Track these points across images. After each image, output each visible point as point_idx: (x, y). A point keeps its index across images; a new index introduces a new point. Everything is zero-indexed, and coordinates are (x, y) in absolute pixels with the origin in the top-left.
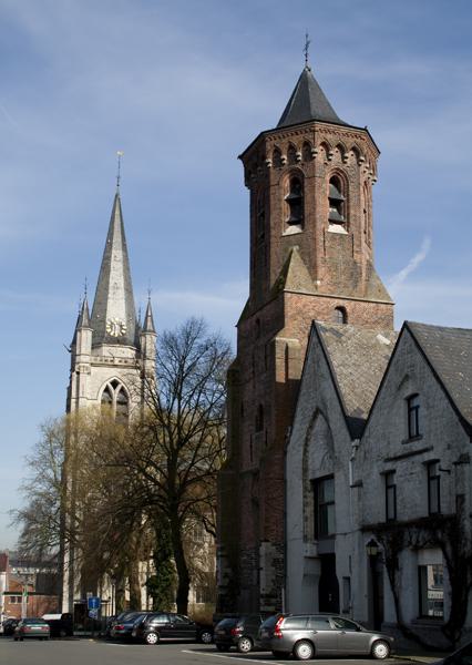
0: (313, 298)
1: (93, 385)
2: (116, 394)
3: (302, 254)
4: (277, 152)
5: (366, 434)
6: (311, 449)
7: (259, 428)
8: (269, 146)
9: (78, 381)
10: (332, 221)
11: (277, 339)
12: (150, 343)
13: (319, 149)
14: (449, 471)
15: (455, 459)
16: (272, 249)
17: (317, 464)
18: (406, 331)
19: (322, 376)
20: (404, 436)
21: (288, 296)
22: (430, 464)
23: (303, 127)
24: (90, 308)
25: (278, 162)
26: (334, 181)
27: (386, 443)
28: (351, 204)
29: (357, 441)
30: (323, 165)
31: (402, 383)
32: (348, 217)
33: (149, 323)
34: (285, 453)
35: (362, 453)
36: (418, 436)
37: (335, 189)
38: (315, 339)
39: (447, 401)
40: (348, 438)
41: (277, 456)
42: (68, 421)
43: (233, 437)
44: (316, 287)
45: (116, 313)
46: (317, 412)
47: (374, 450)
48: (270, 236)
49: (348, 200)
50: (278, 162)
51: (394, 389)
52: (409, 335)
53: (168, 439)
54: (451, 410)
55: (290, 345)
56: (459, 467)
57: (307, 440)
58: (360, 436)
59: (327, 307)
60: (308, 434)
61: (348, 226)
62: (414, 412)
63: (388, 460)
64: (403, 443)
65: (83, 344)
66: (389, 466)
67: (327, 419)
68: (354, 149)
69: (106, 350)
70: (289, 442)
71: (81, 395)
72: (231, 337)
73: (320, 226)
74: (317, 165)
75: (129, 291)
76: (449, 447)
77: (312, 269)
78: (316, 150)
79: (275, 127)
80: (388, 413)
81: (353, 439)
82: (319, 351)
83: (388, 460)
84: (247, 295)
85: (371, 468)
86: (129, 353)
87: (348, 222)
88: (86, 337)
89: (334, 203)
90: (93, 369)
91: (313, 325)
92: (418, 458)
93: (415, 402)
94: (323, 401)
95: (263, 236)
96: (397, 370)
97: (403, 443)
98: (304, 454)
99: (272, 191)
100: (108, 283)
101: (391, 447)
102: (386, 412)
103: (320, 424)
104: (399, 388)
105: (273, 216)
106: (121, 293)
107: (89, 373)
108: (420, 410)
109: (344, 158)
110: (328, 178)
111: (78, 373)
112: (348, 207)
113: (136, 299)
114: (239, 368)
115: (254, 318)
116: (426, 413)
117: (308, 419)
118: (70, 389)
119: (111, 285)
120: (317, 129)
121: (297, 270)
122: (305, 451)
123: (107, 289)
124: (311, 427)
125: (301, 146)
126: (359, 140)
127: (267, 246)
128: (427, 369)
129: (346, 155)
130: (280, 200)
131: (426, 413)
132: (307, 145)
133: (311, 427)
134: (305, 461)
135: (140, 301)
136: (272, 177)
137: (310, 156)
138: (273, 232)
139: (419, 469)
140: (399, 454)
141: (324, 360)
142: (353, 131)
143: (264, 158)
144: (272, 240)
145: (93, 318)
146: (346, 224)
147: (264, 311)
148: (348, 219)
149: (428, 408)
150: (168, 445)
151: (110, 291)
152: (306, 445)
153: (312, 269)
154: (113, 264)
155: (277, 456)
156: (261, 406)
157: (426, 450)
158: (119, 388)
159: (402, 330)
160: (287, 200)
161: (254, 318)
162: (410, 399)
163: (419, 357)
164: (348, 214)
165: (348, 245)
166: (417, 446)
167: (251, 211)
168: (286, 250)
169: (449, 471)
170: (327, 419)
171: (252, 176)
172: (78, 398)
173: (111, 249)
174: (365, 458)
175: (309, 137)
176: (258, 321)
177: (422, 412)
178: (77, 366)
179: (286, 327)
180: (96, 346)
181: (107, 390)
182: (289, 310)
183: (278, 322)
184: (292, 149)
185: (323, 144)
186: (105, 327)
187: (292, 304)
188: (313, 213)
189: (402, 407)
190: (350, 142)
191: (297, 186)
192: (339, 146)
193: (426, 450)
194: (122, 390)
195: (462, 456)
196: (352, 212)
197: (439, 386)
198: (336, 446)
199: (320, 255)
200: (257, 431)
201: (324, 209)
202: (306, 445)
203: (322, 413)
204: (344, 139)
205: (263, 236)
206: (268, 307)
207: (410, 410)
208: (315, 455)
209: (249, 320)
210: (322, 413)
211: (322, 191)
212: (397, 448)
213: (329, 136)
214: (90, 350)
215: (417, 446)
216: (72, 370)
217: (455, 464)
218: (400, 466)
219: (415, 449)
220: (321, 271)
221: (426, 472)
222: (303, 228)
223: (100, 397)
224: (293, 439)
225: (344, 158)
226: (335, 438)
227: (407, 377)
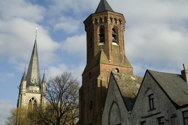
0: (108, 65)
1: (26, 98)
2: (33, 102)
3: (105, 52)
4: (96, 20)
5: (134, 109)
6: (111, 115)
7: (91, 108)
8: (93, 18)
9: (21, 98)
10: (113, 41)
11: (98, 78)
12: (44, 86)
13: (109, 19)
14: (168, 121)
15: (171, 116)
16: (95, 50)
17: (114, 120)
18: (147, 72)
19: (115, 90)
20: (148, 109)
21: (101, 64)
22: (159, 119)
23: (104, 13)
24: (26, 75)
25: (96, 23)
26: (113, 29)
27: (142, 112)
28: (119, 36)
29: (130, 112)
30: (111, 25)
31: (147, 90)
32: (118, 40)
33: (44, 80)
34: (101, 117)
35: (132, 116)
36: (154, 109)
37: (113, 32)
38: (112, 78)
39: (165, 96)
40: (126, 111)
41: (99, 118)
42: (17, 111)
43: (81, 112)
44: (109, 62)
45: (34, 76)
46: (114, 102)
47: (137, 115)
48: (94, 46)
49: (118, 35)
50: (96, 23)
51: (144, 93)
52: (149, 74)
53: (57, 114)
54: (167, 98)
55: (102, 80)
56: (173, 119)
57: (110, 112)
58: (131, 110)
59: (113, 68)
60: (110, 110)
61: (118, 43)
62: (151, 101)
63: (143, 118)
64: (148, 111)
65: (24, 86)
66: (143, 120)
67: (118, 105)
68: (119, 20)
69: (30, 88)
70: (103, 113)
71: (22, 102)
72: (80, 80)
73: (110, 43)
74: (108, 24)
75: (38, 70)
76: (168, 112)
77: (108, 56)
78: (108, 20)
79: (94, 12)
80: (142, 101)
81: (128, 111)
82: (114, 81)
83: (143, 118)
84: (86, 64)
85: (136, 121)
86: (38, 89)
87: (118, 42)
88: (25, 83)
89: (114, 36)
90: (26, 94)
91: (112, 73)
92: (155, 116)
93: (152, 97)
94: (116, 98)
95: (91, 46)
96: (144, 86)
97: (148, 111)
98: (109, 117)
99: (95, 31)
100: (32, 67)
101: (143, 113)
102: (141, 101)
103: (115, 106)
104: (146, 92)
105: (95, 39)
106: (36, 70)
107: (25, 95)
108: (154, 100)
109: (116, 22)
110: (112, 28)
111: (22, 95)
112: (118, 37)
113: (40, 72)
114: (83, 89)
115: (89, 72)
116: (157, 100)
117: (110, 105)
118: (19, 99)
119: (33, 68)
120: (108, 13)
121: (103, 57)
122: (109, 116)
123: (32, 69)
124: (111, 107)
125: (103, 18)
126: (120, 17)
127: (93, 49)
128: (157, 85)
129: (117, 21)
130: (97, 35)
131: (157, 100)
132: (106, 18)
133: (111, 107)
134: (109, 119)
135: (42, 72)
136: (94, 28)
137: (106, 21)
138: (95, 45)
139: (156, 120)
140: (146, 116)
141: (116, 84)
142: (119, 15)
143: (92, 22)
144: (95, 47)
145: (27, 77)
146: (118, 43)
147: (92, 70)
148: (118, 41)
149: (158, 98)
150: (57, 116)
151: (33, 69)
152: (109, 114)
153: (108, 56)
154: (34, 61)
155: (99, 118)
156: (91, 101)
157: (158, 113)
158: (34, 100)
159: (146, 72)
160: (99, 35)
161: (89, 72)
162: (149, 96)
163: (153, 81)
164: (118, 39)
165: (119, 49)
166: (154, 112)
167: (87, 38)
168: (100, 50)
169: (168, 121)
170: (118, 105)
171: (88, 27)
172: (21, 103)
173: (33, 57)
174: (133, 117)
175: (106, 16)
176: (90, 73)
177: (155, 100)
178: (21, 93)
179: (101, 75)
180: (28, 86)
181: (30, 101)
182: (101, 69)
183: (98, 73)
184: (101, 19)
185: (110, 18)
186: (30, 81)
187: (102, 67)
188: (108, 39)
189: (147, 99)
190: (118, 18)
191: (102, 31)
192: (115, 19)
193: (158, 113)
194: (35, 101)
195: (173, 115)
196: (119, 39)
197: (162, 91)
198: (121, 114)
199: (110, 51)
200: (90, 110)
201: (111, 38)
202: (109, 114)
203: (116, 103)
204: (117, 17)
205: (91, 46)
206: (94, 68)
207: (150, 100)
208: (113, 117)
209: (87, 73)
210: (116, 103)
211: (110, 33)
212: (146, 113)
213: (112, 16)
214: (25, 87)
215: (154, 112)
216: (20, 94)
217: (171, 118)
218: (148, 120)
219: (153, 113)
220: (111, 57)
221: (158, 121)
222: (105, 43)
223: (28, 103)
224: (104, 112)
225: (116, 22)
226: (108, 113)
227: (149, 88)
